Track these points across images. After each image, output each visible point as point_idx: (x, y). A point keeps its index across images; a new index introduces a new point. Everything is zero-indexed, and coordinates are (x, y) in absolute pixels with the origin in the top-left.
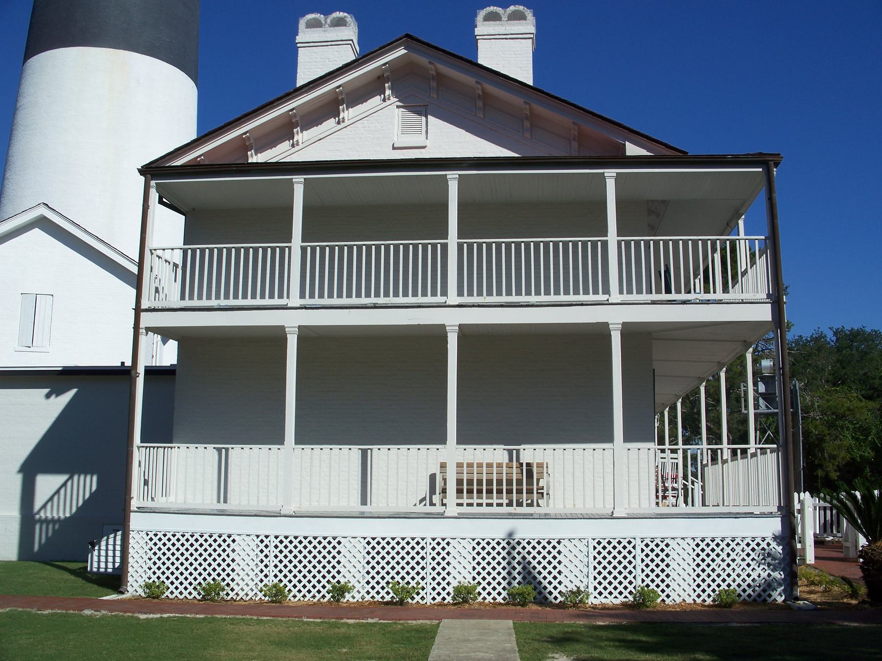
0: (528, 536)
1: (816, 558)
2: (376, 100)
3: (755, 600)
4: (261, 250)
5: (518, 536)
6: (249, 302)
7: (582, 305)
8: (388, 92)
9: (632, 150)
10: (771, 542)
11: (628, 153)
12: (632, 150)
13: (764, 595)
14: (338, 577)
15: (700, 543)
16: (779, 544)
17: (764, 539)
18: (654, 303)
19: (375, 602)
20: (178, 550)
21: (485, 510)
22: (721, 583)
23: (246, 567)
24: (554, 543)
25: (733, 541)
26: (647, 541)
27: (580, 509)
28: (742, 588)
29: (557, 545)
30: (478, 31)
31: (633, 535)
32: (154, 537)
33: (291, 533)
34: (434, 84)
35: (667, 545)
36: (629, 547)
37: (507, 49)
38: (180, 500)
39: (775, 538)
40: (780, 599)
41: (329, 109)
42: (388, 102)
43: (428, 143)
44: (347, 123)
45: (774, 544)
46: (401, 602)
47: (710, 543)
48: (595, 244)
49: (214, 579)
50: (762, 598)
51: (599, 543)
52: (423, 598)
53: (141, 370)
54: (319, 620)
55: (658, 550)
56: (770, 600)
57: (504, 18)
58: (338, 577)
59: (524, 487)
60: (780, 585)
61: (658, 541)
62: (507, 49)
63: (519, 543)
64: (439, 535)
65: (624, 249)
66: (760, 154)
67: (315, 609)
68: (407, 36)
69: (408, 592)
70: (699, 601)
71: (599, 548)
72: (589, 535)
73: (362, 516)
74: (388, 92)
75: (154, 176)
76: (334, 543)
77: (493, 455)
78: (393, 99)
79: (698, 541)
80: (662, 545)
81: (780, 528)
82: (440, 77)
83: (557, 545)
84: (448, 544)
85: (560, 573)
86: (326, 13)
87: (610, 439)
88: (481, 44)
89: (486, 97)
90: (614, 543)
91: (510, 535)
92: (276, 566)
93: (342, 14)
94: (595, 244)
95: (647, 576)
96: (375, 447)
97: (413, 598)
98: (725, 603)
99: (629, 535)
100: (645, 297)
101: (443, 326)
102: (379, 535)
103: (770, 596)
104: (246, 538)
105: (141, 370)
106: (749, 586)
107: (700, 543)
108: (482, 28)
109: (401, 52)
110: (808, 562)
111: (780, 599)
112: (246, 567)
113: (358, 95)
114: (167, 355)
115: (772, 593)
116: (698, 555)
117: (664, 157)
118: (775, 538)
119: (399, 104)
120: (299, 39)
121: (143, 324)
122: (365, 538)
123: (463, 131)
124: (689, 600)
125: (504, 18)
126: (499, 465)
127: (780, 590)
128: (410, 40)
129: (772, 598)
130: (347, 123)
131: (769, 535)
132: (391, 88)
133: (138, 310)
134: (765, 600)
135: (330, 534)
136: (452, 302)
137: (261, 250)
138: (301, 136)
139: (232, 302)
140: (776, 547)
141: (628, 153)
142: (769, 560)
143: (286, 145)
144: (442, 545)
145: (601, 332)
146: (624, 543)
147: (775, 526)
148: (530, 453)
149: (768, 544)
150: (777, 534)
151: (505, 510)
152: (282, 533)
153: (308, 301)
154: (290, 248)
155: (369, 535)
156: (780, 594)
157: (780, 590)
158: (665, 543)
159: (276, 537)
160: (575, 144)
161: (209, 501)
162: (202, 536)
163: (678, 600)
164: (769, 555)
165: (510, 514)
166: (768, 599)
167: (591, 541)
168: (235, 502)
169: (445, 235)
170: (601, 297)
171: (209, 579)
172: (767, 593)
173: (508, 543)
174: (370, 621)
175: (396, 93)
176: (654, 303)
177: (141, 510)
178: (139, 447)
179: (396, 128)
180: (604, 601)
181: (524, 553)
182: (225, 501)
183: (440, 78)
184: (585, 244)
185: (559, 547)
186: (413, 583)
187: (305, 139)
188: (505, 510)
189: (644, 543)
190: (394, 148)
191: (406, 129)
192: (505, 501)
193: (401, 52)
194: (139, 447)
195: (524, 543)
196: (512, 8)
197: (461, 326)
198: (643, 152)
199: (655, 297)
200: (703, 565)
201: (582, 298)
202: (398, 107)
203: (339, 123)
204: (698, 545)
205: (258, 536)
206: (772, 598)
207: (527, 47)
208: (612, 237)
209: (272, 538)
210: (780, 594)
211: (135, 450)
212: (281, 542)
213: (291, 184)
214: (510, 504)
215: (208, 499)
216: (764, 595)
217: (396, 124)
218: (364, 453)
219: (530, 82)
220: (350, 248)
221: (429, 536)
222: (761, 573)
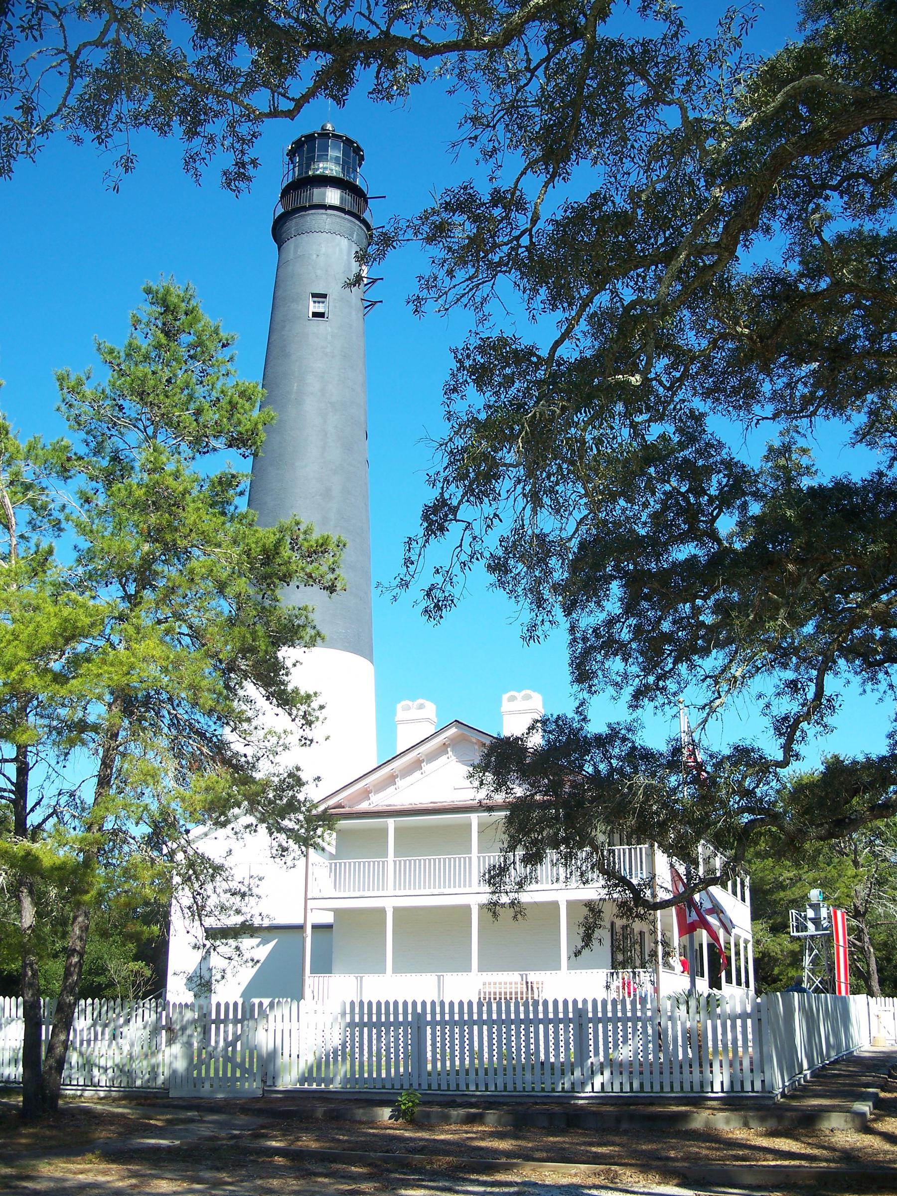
2: (445, 757)
8: (450, 753)
88: (505, 718)
121: (309, 907)
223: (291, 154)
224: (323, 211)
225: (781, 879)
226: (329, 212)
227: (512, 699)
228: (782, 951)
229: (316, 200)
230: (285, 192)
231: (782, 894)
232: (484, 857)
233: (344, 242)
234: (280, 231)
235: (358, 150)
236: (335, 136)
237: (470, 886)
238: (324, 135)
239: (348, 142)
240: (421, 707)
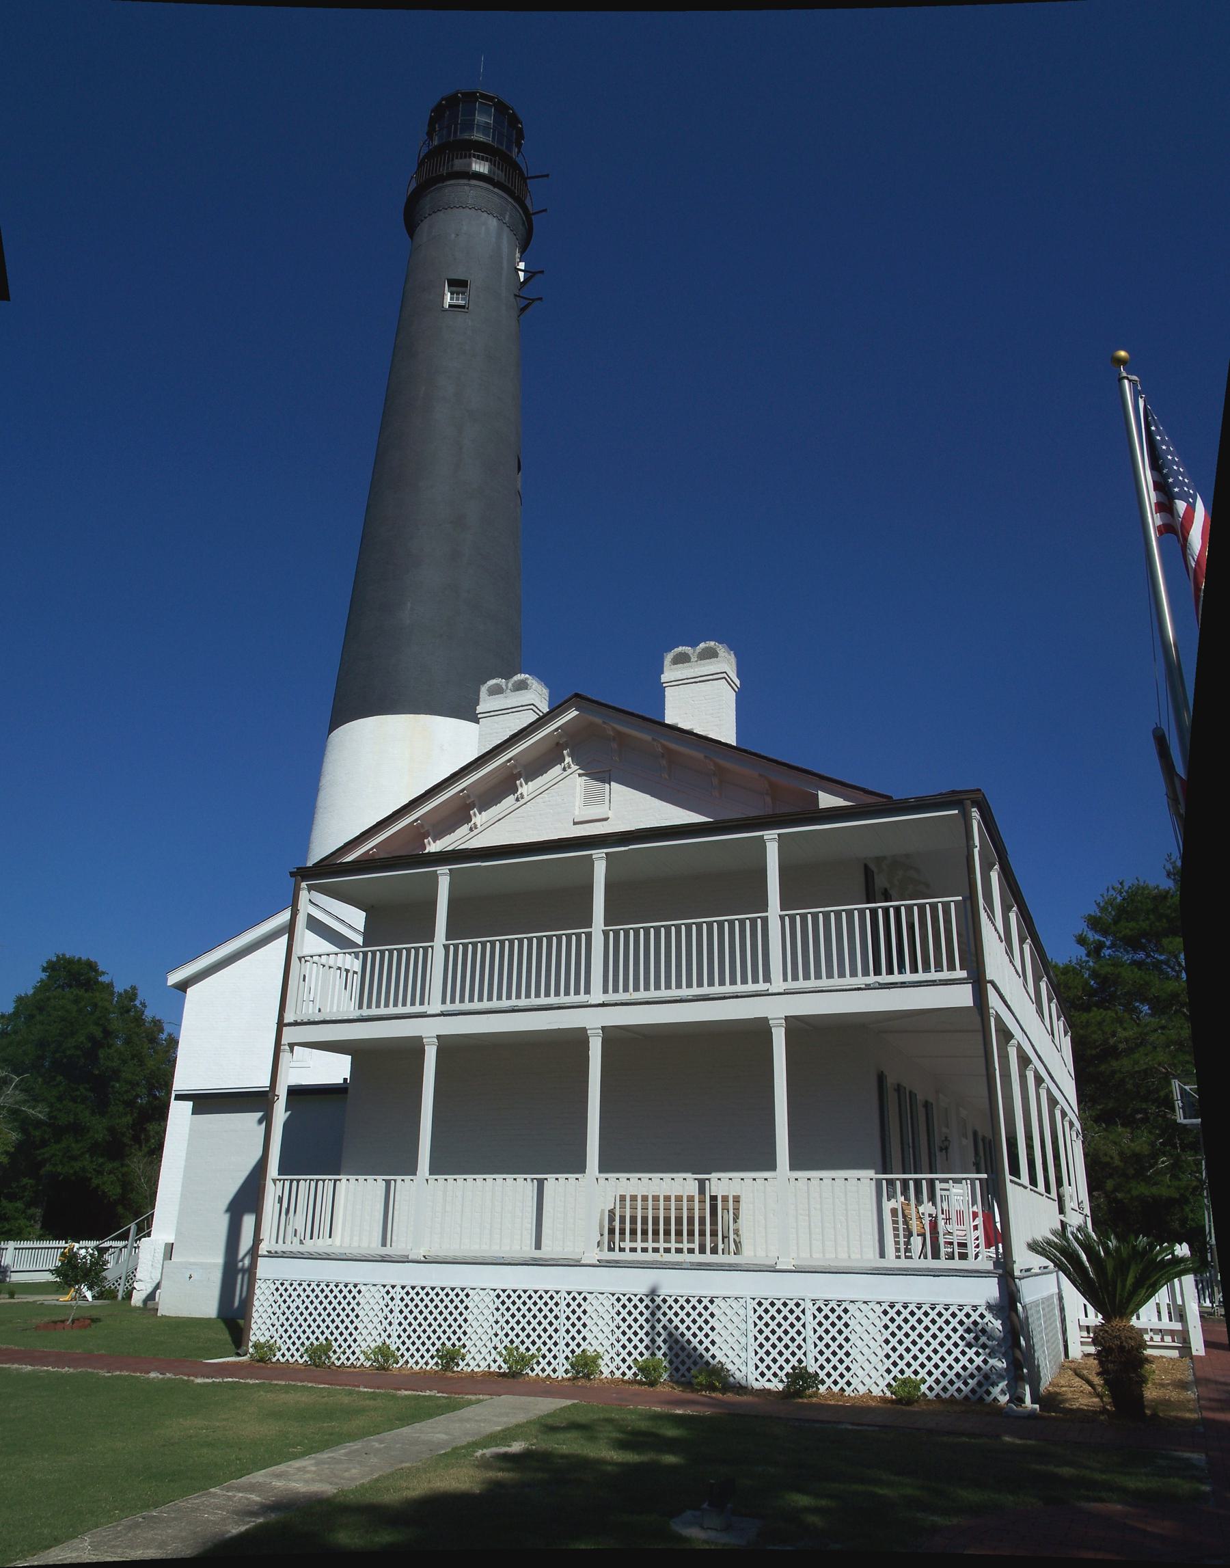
0: (676, 1292)
1: (1207, 1344)
2: (557, 769)
3: (966, 1397)
4: (564, 938)
5: (663, 1292)
6: (552, 1000)
7: (737, 997)
8: (568, 760)
9: (827, 800)
10: (985, 1313)
11: (822, 805)
12: (827, 800)
13: (980, 1391)
14: (584, 1345)
15: (888, 1309)
16: (997, 1317)
17: (975, 1308)
18: (868, 987)
19: (490, 1373)
20: (773, 1318)
21: (650, 1256)
22: (919, 1369)
23: (600, 1335)
24: (706, 1302)
25: (933, 1309)
26: (820, 1304)
27: (818, 1260)
28: (948, 1378)
29: (709, 1305)
31: (802, 1295)
32: (282, 1287)
33: (419, 1283)
35: (846, 1311)
36: (798, 1312)
37: (702, 699)
39: (989, 1307)
40: (1004, 1399)
42: (569, 771)
43: (610, 814)
44: (526, 798)
45: (989, 1316)
46: (513, 1375)
47: (902, 1310)
48: (753, 922)
49: (326, 1339)
50: (977, 1396)
51: (760, 1304)
52: (554, 1371)
53: (282, 1092)
54: (362, 1389)
55: (835, 1315)
56: (989, 1399)
58: (584, 1345)
59: (708, 1230)
60: (1002, 1378)
61: (833, 1304)
62: (702, 699)
63: (664, 1301)
64: (574, 1288)
66: (954, 792)
67: (421, 1379)
68: (577, 695)
69: (524, 1361)
70: (836, 1389)
71: (760, 1311)
72: (748, 1293)
73: (383, 1259)
74: (568, 760)
75: (304, 878)
76: (579, 1299)
77: (678, 1185)
78: (574, 767)
79: (885, 1306)
80: (839, 1311)
81: (997, 1294)
82: (620, 736)
83: (709, 1305)
84: (585, 1299)
85: (584, 1339)
87: (772, 1166)
88: (669, 692)
89: (669, 754)
90: (779, 1304)
91: (653, 1294)
92: (556, 1331)
95: (821, 1353)
96: (399, 1178)
97: (532, 1370)
98: (906, 1396)
99: (796, 1295)
100: (861, 980)
101: (765, 1020)
102: (510, 1286)
103: (988, 1393)
104: (863, 1307)
105: (282, 1092)
106: (958, 1375)
107: (888, 1309)
109: (573, 713)
110: (1194, 1353)
111: (1004, 1399)
112: (600, 1335)
113: (536, 766)
114: (334, 1069)
115: (991, 1389)
116: (820, 1324)
117: (869, 805)
118: (989, 1307)
119: (581, 771)
121: (285, 1040)
122: (384, 1286)
123: (648, 797)
124: (876, 1392)
126: (691, 1199)
127: (1003, 1385)
128: (578, 699)
129: (992, 1397)
130: (526, 798)
131: (981, 1302)
132: (571, 755)
133: (281, 1025)
134: (981, 1399)
135: (458, 1284)
136: (597, 997)
137: (564, 938)
138: (479, 819)
139: (543, 1001)
140: (993, 1320)
141: (822, 805)
142: (983, 1339)
143: (464, 829)
144: (578, 1299)
145: (759, 1030)
146: (791, 1305)
147: (989, 1290)
148: (722, 1184)
149: (982, 1316)
150: (992, 1302)
151: (697, 1258)
152: (409, 1283)
153: (449, 1007)
154: (432, 947)
155: (500, 1286)
156: (1003, 1392)
157: (1003, 1385)
158: (842, 1307)
159: (403, 1288)
160: (768, 799)
161: (371, 1243)
162: (905, 1308)
163: (862, 1390)
164: (983, 1331)
165: (700, 1264)
166: (985, 1396)
167: (750, 1301)
168: (550, 1249)
169: (764, 907)
170: (761, 986)
171: (322, 1338)
172: (984, 1388)
173: (653, 1301)
174: (428, 1393)
175: (576, 760)
176: (868, 987)
177: (271, 1255)
178: (274, 1181)
179: (579, 800)
180: (768, 1386)
181: (670, 1314)
183: (622, 738)
185: (712, 1308)
186: (533, 1350)
187: (484, 820)
188: (697, 1258)
189: (816, 1306)
190: (575, 823)
191: (589, 799)
192: (696, 1246)
193: (573, 713)
194: (274, 1181)
195: (670, 1301)
198: (839, 802)
199: (861, 980)
200: (827, 1339)
201: (739, 988)
202: (580, 775)
203: (517, 800)
204: (885, 1313)
205: (384, 1286)
206: (992, 1397)
209: (398, 1289)
210: (1003, 1392)
211: (269, 1185)
212: (408, 1293)
213: (761, 842)
214: (702, 1250)
215: (371, 1243)
216: (980, 1391)
217: (578, 795)
218: (388, 1182)
220: (678, 928)
221: (564, 1288)
222: (974, 1359)
223: (432, 122)
224: (465, 181)
225: (1112, 1041)
226: (473, 182)
227: (682, 659)
228: (1121, 1154)
229: (456, 168)
230: (421, 164)
231: (1115, 1064)
232: (616, 933)
233: (493, 223)
234: (412, 220)
235: (514, 120)
236: (483, 96)
237: (587, 991)
238: (471, 97)
239: (501, 108)
240: (522, 686)
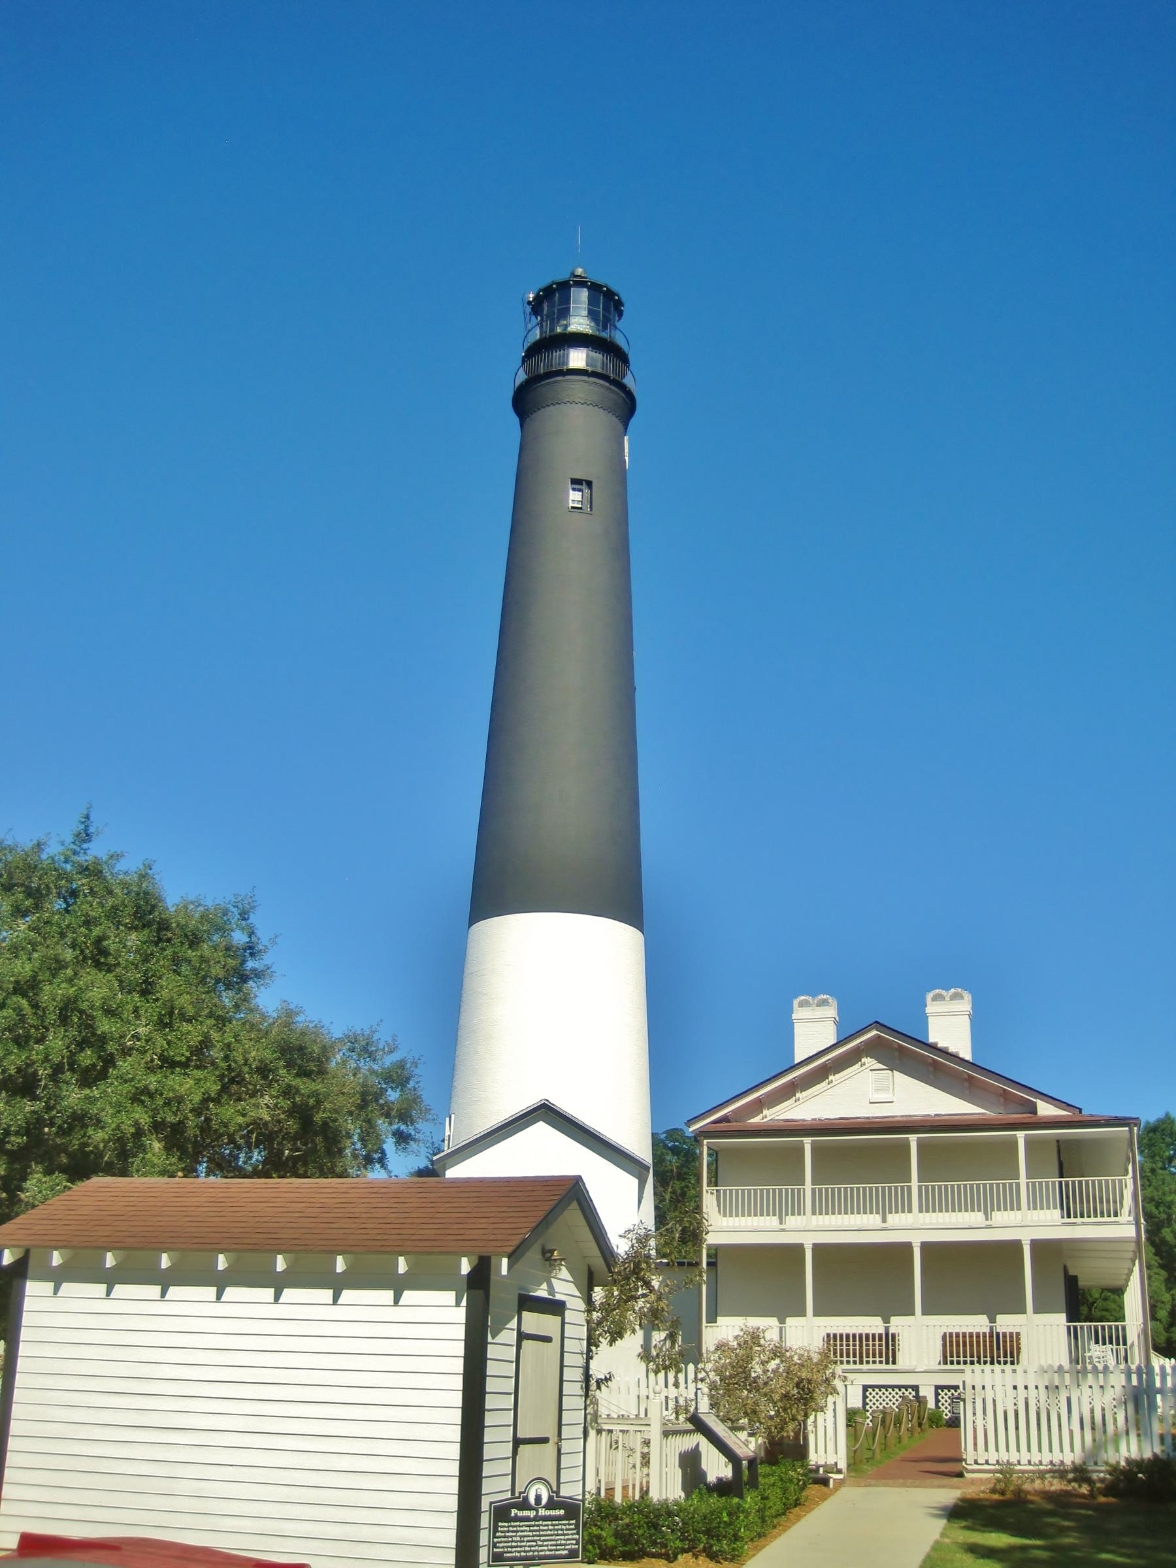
9: (1045, 1109)
30: (928, 1010)
34: (897, 1054)
38: (914, 1363)
41: (821, 1074)
48: (902, 1188)
57: (947, 999)
62: (950, 1026)
65: (1032, 1189)
86: (814, 995)
88: (931, 1020)
93: (825, 997)
94: (902, 1188)
108: (931, 1008)
120: (794, 1016)
125: (947, 999)
136: (920, 1223)
182: (894, 1363)
184: (737, 1191)
196: (953, 990)
197: (1032, 1241)
207: (965, 1022)
208: (1023, 1180)
219: (966, 1054)
